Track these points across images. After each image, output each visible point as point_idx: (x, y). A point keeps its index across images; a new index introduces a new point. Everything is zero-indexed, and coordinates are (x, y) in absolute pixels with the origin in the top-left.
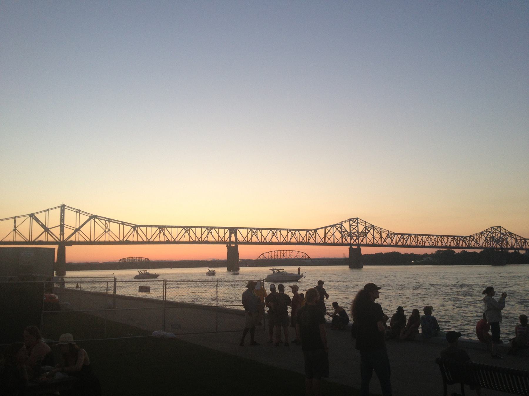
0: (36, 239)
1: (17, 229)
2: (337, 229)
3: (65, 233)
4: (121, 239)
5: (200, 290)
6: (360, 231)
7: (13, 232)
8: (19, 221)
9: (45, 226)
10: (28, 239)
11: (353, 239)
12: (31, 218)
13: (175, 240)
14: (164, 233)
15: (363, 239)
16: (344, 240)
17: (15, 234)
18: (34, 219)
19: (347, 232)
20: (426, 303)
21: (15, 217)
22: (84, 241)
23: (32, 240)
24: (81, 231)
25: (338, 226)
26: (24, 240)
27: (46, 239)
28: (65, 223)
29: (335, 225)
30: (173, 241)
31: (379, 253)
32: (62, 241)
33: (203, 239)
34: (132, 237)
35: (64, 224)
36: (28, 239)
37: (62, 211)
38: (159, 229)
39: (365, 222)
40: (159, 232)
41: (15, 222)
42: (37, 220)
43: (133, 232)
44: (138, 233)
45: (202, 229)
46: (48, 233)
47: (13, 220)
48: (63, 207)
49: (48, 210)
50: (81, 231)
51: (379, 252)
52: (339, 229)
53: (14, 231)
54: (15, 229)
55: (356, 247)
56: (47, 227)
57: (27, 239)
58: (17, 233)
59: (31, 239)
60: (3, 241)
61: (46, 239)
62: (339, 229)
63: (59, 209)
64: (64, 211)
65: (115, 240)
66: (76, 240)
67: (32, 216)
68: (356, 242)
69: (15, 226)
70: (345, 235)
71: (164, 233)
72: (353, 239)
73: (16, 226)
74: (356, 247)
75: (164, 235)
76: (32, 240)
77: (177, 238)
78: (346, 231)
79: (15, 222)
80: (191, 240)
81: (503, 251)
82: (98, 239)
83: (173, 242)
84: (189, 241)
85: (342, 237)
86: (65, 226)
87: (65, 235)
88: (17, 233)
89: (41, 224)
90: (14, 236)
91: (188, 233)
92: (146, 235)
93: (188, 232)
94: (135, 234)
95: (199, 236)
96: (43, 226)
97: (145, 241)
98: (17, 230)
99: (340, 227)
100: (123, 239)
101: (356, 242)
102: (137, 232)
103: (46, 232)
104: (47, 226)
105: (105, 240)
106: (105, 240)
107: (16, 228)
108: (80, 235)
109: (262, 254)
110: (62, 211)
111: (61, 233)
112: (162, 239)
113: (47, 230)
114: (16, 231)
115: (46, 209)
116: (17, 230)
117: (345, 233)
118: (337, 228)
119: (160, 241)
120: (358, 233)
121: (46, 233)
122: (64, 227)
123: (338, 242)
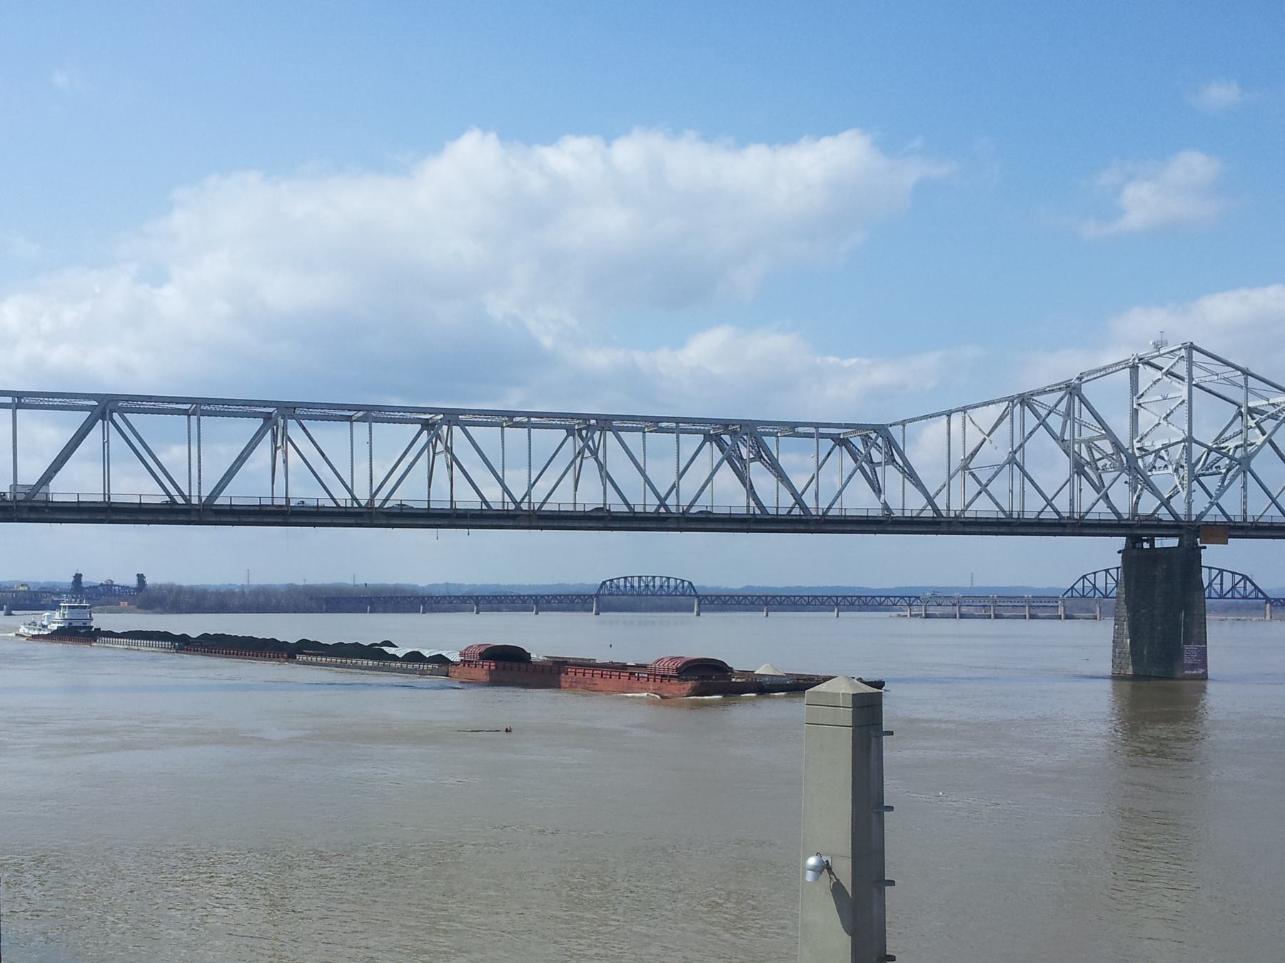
0: (691, 506)
2: (1043, 423)
4: (363, 495)
6: (1207, 434)
11: (1155, 491)
13: (662, 503)
14: (602, 467)
15: (1222, 489)
16: (1089, 495)
17: (108, 428)
19: (1116, 445)
23: (200, 497)
25: (1050, 399)
27: (279, 492)
29: (1025, 400)
33: (685, 502)
34: (573, 489)
38: (708, 443)
39: (1246, 373)
40: (576, 458)
43: (426, 445)
44: (454, 458)
51: (431, 583)
52: (1055, 422)
55: (1173, 543)
62: (1055, 422)
65: (484, 501)
66: (287, 499)
68: (1111, 506)
70: (1100, 464)
71: (602, 467)
72: (1155, 491)
74: (1173, 543)
75: (606, 477)
76: (200, 497)
77: (528, 494)
78: (1109, 434)
80: (617, 506)
85: (1079, 468)
91: (596, 459)
93: (594, 453)
94: (441, 461)
95: (663, 475)
97: (639, 509)
99: (1062, 407)
101: (1111, 506)
102: (448, 450)
109: (1084, 577)
112: (590, 495)
113: (1258, 425)
117: (1099, 449)
118: (1043, 413)
120: (1188, 450)
123: (1049, 515)
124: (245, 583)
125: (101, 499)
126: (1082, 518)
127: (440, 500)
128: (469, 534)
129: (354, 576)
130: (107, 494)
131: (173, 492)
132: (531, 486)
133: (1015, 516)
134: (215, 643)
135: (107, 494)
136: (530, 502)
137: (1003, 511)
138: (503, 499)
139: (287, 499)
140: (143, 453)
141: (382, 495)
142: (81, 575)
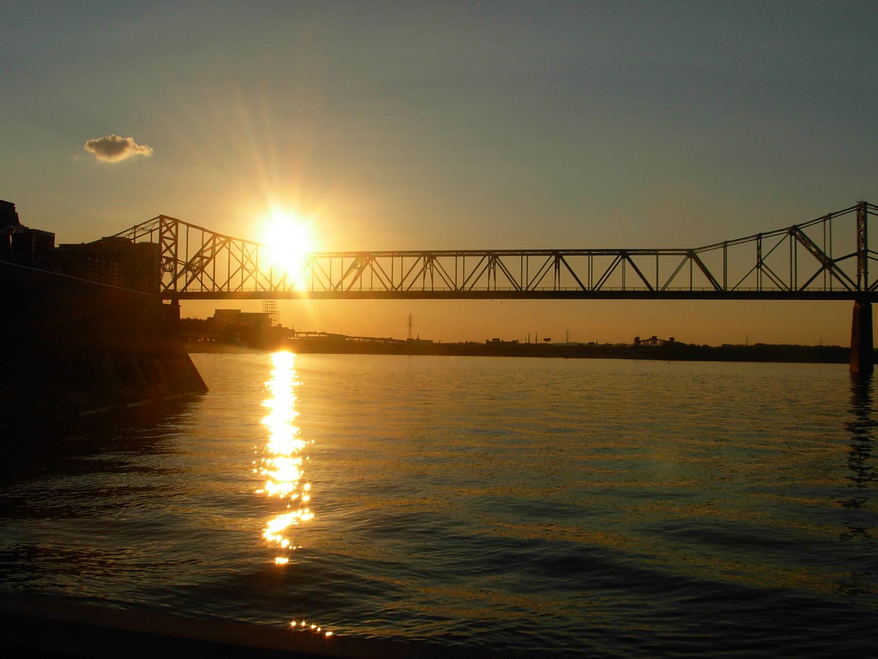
1: (764, 261)
3: (869, 270)
5: (517, 446)
7: (756, 268)
8: (767, 243)
9: (824, 254)
10: (789, 286)
12: (793, 237)
18: (800, 241)
20: (590, 611)
21: (759, 237)
22: (842, 290)
23: (796, 288)
24: (206, 273)
26: (847, 287)
27: (828, 286)
28: (869, 248)
30: (272, 290)
31: (833, 347)
32: (863, 289)
35: (866, 250)
36: (789, 286)
37: (862, 219)
41: (759, 248)
42: (807, 242)
45: (458, 257)
46: (832, 272)
47: (754, 243)
48: (862, 209)
49: (829, 216)
50: (206, 273)
53: (758, 268)
54: (760, 264)
56: (829, 257)
57: (784, 285)
58: (766, 274)
59: (794, 286)
60: (736, 290)
61: (828, 286)
63: (854, 214)
64: (865, 218)
67: (794, 231)
69: (759, 256)
73: (761, 257)
76: (796, 288)
77: (401, 284)
79: (759, 248)
81: (210, 339)
82: (598, 286)
83: (591, 291)
84: (431, 290)
86: (869, 254)
87: (869, 275)
88: (766, 274)
89: (814, 250)
90: (759, 280)
92: (391, 280)
96: (819, 255)
98: (765, 266)
100: (463, 287)
103: (827, 270)
104: (828, 254)
105: (488, 288)
106: (488, 288)
107: (761, 260)
108: (268, 281)
110: (862, 219)
111: (859, 270)
113: (828, 264)
114: (761, 270)
115: (826, 214)
116: (765, 266)
119: (258, 290)
121: (827, 271)
122: (866, 257)
124: (746, 344)
125: (621, 290)
126: (593, 290)
127: (428, 287)
128: (502, 303)
129: (747, 336)
130: (624, 287)
131: (782, 286)
132: (403, 281)
133: (524, 289)
134: (113, 461)
135: (624, 287)
136: (402, 288)
137: (788, 288)
138: (256, 287)
139: (831, 288)
140: (444, 275)
141: (533, 285)
142: (639, 338)
